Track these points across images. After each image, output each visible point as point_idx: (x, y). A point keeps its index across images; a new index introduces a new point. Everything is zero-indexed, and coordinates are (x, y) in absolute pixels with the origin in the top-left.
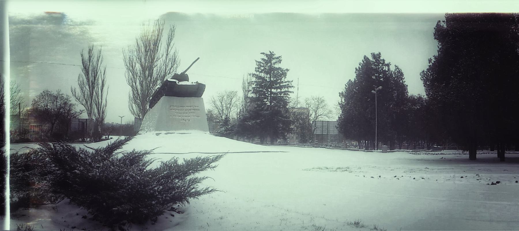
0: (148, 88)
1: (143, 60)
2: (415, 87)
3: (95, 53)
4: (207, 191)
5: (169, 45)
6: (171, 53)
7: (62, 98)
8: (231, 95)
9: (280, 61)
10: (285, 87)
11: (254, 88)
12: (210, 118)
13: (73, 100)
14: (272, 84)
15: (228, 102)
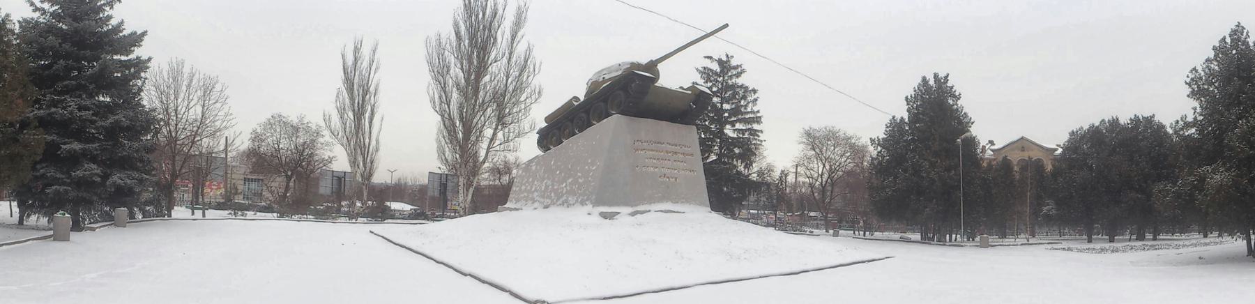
3: (366, 52)
6: (520, 49)
7: (307, 130)
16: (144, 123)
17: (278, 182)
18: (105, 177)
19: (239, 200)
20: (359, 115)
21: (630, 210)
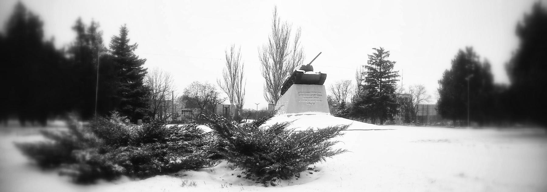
0: (279, 79)
1: (275, 55)
2: (501, 77)
4: (340, 152)
5: (296, 43)
6: (298, 50)
8: (347, 84)
9: (388, 55)
10: (392, 76)
11: (366, 78)
12: (330, 103)
13: (218, 90)
14: (381, 75)
15: (345, 89)
16: (147, 91)
17: (196, 112)
18: (134, 110)
19: (180, 119)
20: (234, 77)
21: (295, 114)
